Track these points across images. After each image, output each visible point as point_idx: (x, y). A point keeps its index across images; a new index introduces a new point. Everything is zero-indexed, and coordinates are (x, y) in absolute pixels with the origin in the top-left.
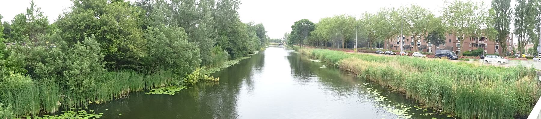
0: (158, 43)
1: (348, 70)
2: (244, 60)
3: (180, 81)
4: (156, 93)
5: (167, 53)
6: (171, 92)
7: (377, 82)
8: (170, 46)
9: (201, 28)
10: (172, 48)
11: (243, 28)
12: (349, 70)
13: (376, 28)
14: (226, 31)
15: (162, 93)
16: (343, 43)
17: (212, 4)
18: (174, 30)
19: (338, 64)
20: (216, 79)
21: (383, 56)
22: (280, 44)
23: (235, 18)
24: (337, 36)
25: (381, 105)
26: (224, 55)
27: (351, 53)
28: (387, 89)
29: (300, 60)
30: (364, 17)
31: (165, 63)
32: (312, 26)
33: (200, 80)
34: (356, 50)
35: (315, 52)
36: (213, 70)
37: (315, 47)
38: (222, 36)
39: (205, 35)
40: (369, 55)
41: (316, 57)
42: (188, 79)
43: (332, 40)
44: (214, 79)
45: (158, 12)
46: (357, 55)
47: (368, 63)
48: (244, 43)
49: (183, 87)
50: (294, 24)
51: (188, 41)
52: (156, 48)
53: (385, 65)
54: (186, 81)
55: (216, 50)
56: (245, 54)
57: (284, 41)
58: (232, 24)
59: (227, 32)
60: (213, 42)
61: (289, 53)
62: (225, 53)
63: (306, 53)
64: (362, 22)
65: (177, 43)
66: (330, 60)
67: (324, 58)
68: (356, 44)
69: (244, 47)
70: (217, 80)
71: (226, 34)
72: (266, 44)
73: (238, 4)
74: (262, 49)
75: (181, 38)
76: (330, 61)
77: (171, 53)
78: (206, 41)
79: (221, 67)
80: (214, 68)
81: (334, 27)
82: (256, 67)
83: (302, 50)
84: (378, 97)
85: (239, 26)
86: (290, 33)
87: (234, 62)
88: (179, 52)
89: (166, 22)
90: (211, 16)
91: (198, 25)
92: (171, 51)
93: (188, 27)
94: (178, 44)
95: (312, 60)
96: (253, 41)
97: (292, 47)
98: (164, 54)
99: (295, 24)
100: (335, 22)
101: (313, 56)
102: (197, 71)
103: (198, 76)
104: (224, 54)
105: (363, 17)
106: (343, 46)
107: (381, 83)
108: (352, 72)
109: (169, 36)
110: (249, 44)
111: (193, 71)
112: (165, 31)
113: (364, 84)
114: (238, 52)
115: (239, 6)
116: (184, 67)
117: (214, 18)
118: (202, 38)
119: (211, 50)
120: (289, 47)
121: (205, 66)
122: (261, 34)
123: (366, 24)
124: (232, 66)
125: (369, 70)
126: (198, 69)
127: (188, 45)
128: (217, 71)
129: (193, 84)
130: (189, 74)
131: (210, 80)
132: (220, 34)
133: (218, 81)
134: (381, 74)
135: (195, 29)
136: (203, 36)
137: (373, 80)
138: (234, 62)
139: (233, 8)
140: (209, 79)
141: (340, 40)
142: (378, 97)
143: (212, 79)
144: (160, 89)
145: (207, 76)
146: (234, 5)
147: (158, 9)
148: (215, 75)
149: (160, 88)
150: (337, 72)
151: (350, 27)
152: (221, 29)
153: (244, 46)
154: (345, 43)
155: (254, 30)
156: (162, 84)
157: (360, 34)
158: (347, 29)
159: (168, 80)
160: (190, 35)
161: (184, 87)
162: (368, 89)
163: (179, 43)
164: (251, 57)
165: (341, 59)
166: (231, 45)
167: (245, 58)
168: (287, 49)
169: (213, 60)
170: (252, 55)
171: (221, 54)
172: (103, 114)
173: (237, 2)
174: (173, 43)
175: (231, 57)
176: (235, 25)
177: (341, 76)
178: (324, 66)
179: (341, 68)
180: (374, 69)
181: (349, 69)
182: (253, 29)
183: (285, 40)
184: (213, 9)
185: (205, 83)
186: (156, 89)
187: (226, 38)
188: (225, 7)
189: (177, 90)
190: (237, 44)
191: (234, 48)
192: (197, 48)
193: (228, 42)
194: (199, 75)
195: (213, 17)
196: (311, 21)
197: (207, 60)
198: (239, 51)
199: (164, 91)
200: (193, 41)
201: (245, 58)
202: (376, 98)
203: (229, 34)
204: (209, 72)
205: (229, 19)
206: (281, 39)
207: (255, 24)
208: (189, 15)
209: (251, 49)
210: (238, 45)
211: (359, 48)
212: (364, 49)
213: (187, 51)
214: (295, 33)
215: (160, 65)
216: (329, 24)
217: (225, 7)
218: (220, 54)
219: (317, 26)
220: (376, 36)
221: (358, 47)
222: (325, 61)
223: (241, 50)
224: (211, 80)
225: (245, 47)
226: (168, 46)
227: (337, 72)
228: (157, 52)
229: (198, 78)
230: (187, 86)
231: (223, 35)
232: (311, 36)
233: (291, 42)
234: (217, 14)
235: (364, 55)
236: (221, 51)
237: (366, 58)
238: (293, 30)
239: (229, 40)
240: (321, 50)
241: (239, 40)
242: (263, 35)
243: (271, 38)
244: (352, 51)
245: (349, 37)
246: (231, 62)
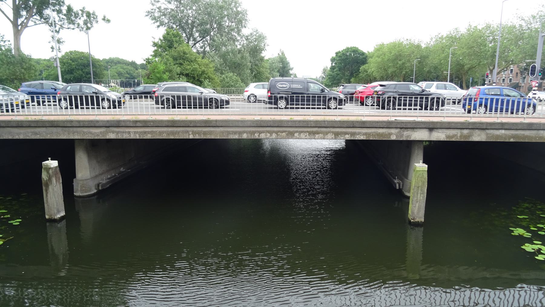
50: (334, 55)
99: (336, 55)
158: (403, 64)
172: (20, 220)
196: (361, 49)
214: (335, 70)
238: (333, 65)
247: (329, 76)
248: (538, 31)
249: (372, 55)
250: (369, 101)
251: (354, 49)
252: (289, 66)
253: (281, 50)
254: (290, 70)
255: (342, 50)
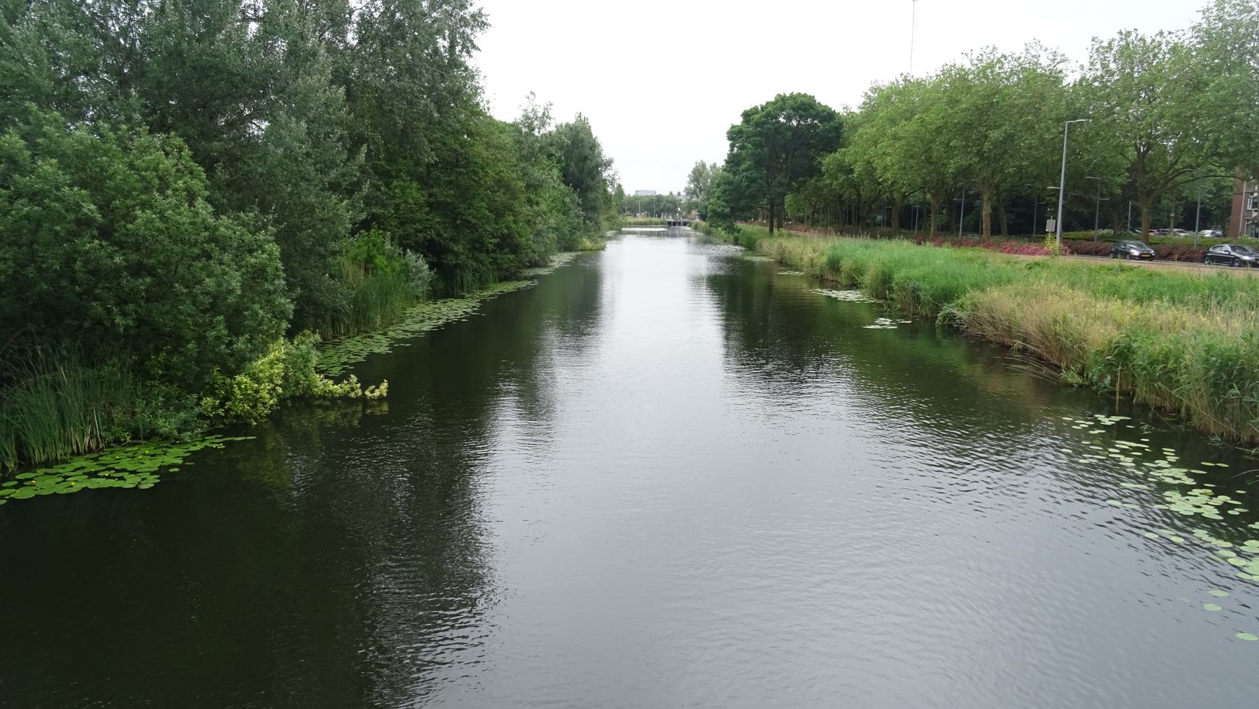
0: (27, 217)
1: (1007, 341)
2: (503, 296)
3: (182, 415)
4: (45, 493)
5: (91, 272)
6: (134, 472)
7: (1179, 414)
8: (105, 233)
9: (279, 142)
10: (121, 245)
11: (497, 148)
12: (1018, 343)
13: (1182, 123)
14: (412, 156)
15: (77, 484)
16: (986, 211)
17: (332, 20)
18: (126, 149)
19: (959, 314)
20: (372, 392)
21: (1219, 275)
22: (671, 219)
23: (456, 93)
24: (955, 177)
25: (1201, 533)
26: (407, 276)
27: (1030, 259)
28: (1243, 452)
29: (770, 288)
30: (1113, 66)
31: (86, 325)
32: (827, 126)
33: (293, 397)
34: (1054, 244)
35: (839, 253)
36: (357, 347)
37: (842, 232)
38: (395, 183)
39: (303, 178)
40: (1131, 269)
41: (843, 279)
42: (226, 399)
43: (928, 196)
44: (360, 392)
45: (13, 44)
46: (1062, 268)
47: (1126, 312)
48: (503, 215)
49: (203, 441)
50: (738, 121)
51: (213, 206)
52: (20, 246)
53: (1237, 323)
54: (214, 408)
55: (369, 251)
56: (507, 269)
57: (690, 207)
58: (440, 123)
59: (418, 163)
60: (345, 211)
61: (711, 259)
62: (412, 264)
63: (797, 257)
64: (1094, 91)
65: (150, 221)
66: (915, 290)
67: (884, 284)
68: (1055, 213)
69: (503, 237)
70: (377, 393)
71: (413, 175)
72: (608, 219)
73: (466, 26)
74: (588, 243)
75: (169, 192)
76: (917, 299)
77: (117, 271)
78: (312, 209)
79: (396, 332)
80: (358, 338)
81: (939, 131)
82: (564, 330)
83: (776, 245)
84: (1184, 490)
85: (478, 134)
86: (721, 163)
87: (457, 309)
88: (166, 265)
89: (72, 105)
90: (332, 82)
91: (265, 125)
92: (118, 260)
93: (209, 134)
94: (158, 224)
95: (826, 292)
96: (543, 207)
97: (731, 229)
98: (73, 281)
100: (948, 103)
101: (831, 273)
102: (272, 356)
103: (280, 382)
104: (406, 269)
105: (1104, 66)
106: (986, 224)
107: (1204, 416)
108: (1033, 353)
109: (94, 183)
110: (528, 222)
111: (250, 360)
112: (69, 152)
113: (1101, 417)
114: (477, 260)
115: (479, 37)
116: (201, 339)
117: (348, 92)
118: (291, 194)
119: (339, 252)
120: (713, 230)
121: (314, 332)
122: (581, 172)
123: (1118, 104)
124: (447, 325)
125: (1135, 345)
126: (280, 349)
127: (216, 229)
128: (377, 350)
129: (256, 420)
130: (232, 374)
131: (340, 398)
132: (386, 176)
133: (381, 399)
134: (1208, 370)
135: (251, 143)
136: (296, 185)
137: (1153, 400)
138: (457, 309)
139: (443, 43)
140: (338, 389)
141: (968, 196)
142: (1184, 494)
143: (353, 390)
144: (68, 469)
145: (326, 377)
146: (447, 33)
147: (10, 23)
148: (368, 371)
149: (65, 462)
150: (953, 355)
151: (1025, 123)
152: (387, 151)
153: (506, 231)
154: (995, 209)
155: (550, 156)
156: (76, 437)
157: (1086, 157)
158: (1010, 138)
159: (110, 414)
160: (222, 174)
161: (206, 443)
162: (1125, 444)
163: (163, 218)
164: (536, 283)
165: (976, 286)
166: (437, 226)
167: (509, 287)
168: (706, 242)
169: (355, 301)
170: (542, 272)
171: (393, 270)
173: (462, 18)
174: (124, 217)
175: (441, 285)
176: (458, 132)
177: (973, 372)
178: (886, 322)
179: (974, 331)
180: (1164, 343)
181: (1018, 338)
182: (541, 149)
183: (695, 199)
184: (341, 47)
185: (319, 413)
186: (40, 472)
187: (415, 193)
188: (403, 38)
189: (169, 460)
190: (468, 222)
191: (456, 242)
192: (269, 242)
193: (427, 213)
194: (285, 378)
195: (342, 90)
197: (326, 299)
198: (483, 256)
199: (93, 475)
200: (241, 209)
201: (509, 287)
202: (1167, 493)
203: (429, 172)
204: (335, 359)
205: (425, 100)
206: (675, 193)
207: (551, 128)
208: (210, 70)
209: (535, 247)
210: (472, 227)
211: (1072, 234)
212: (1102, 237)
213: (209, 257)
214: (743, 166)
215: (58, 339)
216: (913, 115)
217: (403, 38)
218: (388, 270)
219: (855, 128)
220: (1179, 166)
221: (1066, 227)
222: (892, 299)
223: (487, 252)
224: (345, 398)
225: (510, 236)
226: (95, 232)
227: (953, 355)
228: (24, 266)
229: (280, 390)
230: (225, 433)
231: (397, 177)
232: (822, 175)
233: (727, 210)
234: (363, 72)
235: (1102, 267)
236: (390, 258)
237: (1112, 285)
239: (429, 204)
240: (871, 242)
241: (476, 203)
242: (593, 179)
243: (629, 191)
244: (1033, 246)
245: (1021, 178)
246: (444, 310)
247: (723, 187)
248: (1063, 96)
249: (854, 123)
250: (1190, 297)
251: (804, 100)
252: (600, 154)
253: (580, 117)
254: (600, 165)
255: (764, 104)
